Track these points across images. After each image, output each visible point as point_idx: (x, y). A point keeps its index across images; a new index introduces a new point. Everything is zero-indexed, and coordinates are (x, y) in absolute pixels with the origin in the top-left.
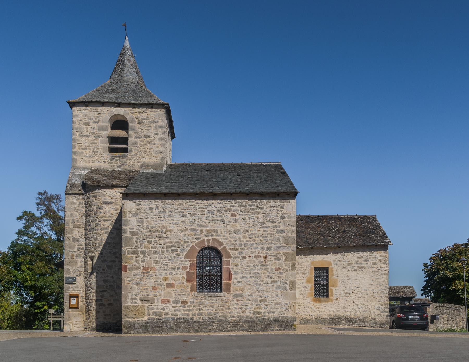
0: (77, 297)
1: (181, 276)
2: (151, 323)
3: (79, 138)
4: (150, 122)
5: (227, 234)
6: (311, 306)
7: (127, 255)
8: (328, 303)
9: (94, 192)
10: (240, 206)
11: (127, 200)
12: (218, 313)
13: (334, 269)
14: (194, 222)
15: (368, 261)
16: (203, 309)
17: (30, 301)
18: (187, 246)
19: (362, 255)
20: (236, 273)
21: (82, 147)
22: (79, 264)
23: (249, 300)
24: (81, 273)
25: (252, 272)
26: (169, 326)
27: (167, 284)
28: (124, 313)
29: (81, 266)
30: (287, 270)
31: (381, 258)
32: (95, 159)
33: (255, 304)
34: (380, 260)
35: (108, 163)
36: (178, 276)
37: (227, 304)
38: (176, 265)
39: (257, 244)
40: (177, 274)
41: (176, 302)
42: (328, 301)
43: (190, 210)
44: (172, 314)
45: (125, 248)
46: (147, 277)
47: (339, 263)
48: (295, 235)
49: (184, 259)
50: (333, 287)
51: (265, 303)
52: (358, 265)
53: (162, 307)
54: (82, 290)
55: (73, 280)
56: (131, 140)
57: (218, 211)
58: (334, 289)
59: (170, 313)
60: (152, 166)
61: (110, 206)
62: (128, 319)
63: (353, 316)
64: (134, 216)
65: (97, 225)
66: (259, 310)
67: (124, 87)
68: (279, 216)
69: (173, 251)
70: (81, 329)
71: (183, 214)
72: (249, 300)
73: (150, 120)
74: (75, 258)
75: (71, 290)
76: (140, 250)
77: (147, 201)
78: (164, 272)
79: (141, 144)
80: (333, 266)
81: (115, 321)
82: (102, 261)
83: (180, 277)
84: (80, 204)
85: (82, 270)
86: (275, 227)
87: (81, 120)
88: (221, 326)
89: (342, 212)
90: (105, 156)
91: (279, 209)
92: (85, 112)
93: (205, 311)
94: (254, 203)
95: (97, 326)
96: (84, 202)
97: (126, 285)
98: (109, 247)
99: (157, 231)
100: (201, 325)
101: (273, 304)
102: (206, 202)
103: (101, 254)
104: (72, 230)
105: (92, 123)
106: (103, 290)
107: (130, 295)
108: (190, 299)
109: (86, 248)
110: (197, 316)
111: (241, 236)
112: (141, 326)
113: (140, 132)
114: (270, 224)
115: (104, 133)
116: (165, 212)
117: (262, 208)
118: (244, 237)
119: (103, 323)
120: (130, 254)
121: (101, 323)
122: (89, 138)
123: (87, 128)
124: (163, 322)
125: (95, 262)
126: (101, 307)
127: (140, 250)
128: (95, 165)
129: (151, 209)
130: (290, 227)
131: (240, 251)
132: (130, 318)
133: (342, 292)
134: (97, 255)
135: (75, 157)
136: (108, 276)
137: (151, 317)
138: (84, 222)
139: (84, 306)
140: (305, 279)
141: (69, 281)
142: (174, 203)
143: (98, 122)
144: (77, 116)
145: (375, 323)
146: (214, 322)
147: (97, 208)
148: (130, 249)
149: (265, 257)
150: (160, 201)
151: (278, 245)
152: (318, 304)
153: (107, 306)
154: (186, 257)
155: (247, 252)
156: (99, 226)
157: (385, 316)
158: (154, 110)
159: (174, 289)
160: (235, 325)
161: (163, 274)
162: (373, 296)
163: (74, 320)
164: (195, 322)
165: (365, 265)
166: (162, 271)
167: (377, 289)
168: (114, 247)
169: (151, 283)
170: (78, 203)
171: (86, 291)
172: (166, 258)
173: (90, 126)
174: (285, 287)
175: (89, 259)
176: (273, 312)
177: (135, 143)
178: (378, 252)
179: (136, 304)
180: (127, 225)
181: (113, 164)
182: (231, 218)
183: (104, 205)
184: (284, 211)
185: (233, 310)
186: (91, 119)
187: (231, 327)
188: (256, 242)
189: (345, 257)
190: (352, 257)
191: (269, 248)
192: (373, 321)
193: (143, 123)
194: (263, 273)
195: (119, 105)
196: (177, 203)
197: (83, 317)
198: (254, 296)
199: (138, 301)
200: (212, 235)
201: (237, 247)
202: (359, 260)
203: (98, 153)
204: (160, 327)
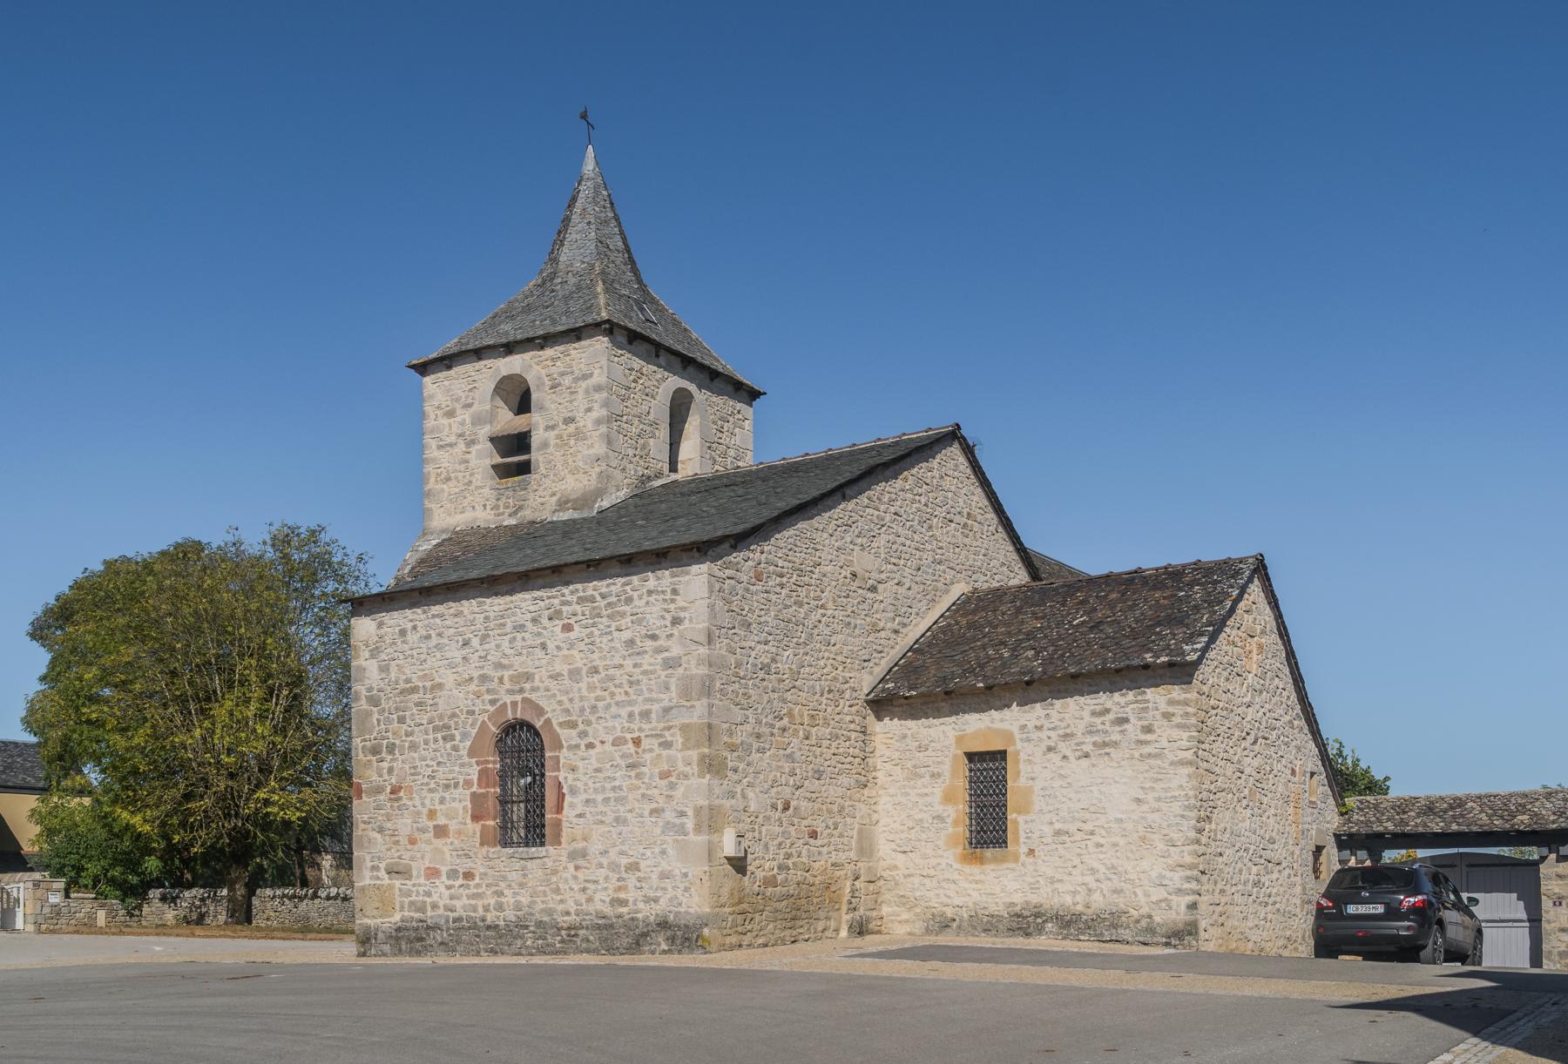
2: (406, 929)
3: (436, 453)
4: (576, 380)
5: (552, 684)
6: (956, 876)
7: (361, 756)
8: (1005, 865)
10: (581, 600)
13: (1023, 756)
15: (1126, 720)
19: (1109, 705)
20: (573, 791)
23: (601, 866)
25: (608, 786)
27: (435, 827)
30: (686, 777)
31: (1171, 709)
34: (1167, 716)
36: (455, 805)
37: (554, 879)
39: (617, 704)
40: (454, 800)
41: (453, 874)
42: (1003, 860)
47: (1035, 735)
50: (1019, 813)
52: (1096, 738)
56: (535, 441)
58: (1021, 819)
59: (441, 904)
60: (575, 501)
63: (1080, 908)
64: (372, 657)
66: (622, 896)
68: (669, 617)
69: (444, 738)
72: (601, 866)
80: (1019, 745)
86: (659, 651)
87: (438, 408)
89: (1151, 560)
90: (486, 491)
91: (668, 596)
93: (509, 899)
94: (613, 588)
99: (414, 690)
100: (499, 936)
101: (654, 876)
105: (460, 405)
107: (368, 858)
108: (479, 869)
110: (495, 913)
111: (583, 685)
114: (649, 643)
117: (629, 600)
118: (591, 688)
124: (428, 927)
131: (581, 727)
133: (1048, 830)
140: (938, 792)
145: (1151, 930)
146: (527, 927)
149: (637, 742)
150: (419, 611)
151: (666, 704)
152: (974, 870)
154: (471, 753)
155: (598, 730)
158: (583, 343)
160: (571, 937)
161: (427, 802)
162: (1143, 839)
164: (489, 928)
165: (1116, 737)
166: (424, 793)
167: (1156, 816)
169: (404, 824)
174: (683, 825)
176: (656, 900)
177: (545, 445)
178: (1159, 689)
184: (680, 602)
185: (567, 895)
186: (457, 400)
187: (562, 941)
188: (618, 698)
189: (1053, 713)
190: (1076, 711)
191: (645, 715)
192: (1144, 923)
194: (632, 788)
195: (509, 348)
198: (613, 853)
199: (382, 873)
200: (521, 691)
202: (1098, 720)
204: (422, 939)
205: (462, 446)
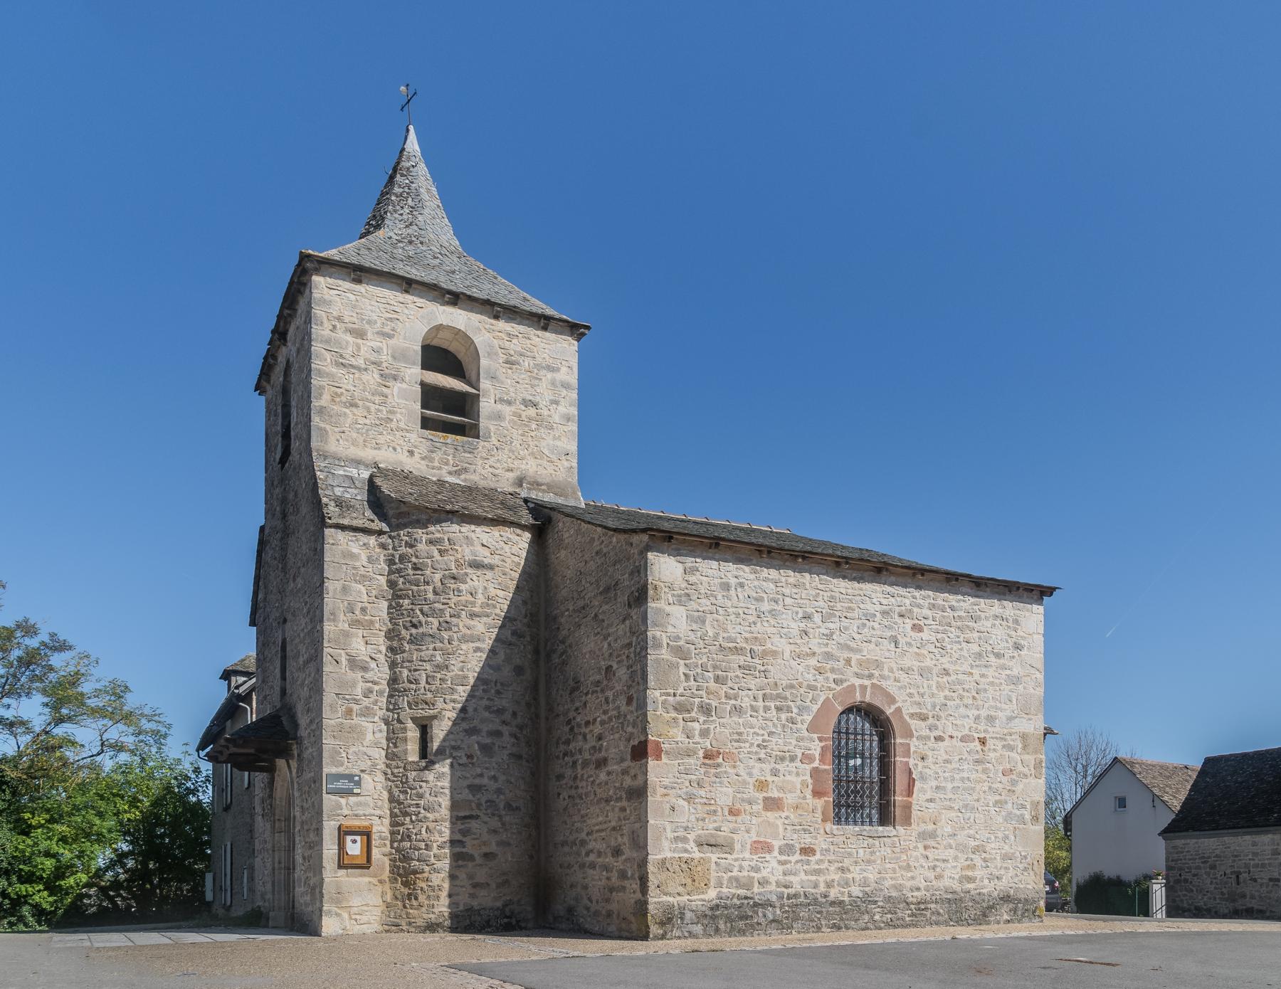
1: (800, 779)
2: (726, 907)
5: (902, 676)
9: (432, 528)
12: (884, 879)
14: (829, 636)
16: (852, 868)
18: (813, 700)
20: (923, 778)
22: (369, 737)
24: (374, 765)
26: (771, 917)
27: (765, 799)
29: (376, 744)
32: (381, 440)
33: (962, 857)
35: (423, 459)
36: (792, 778)
38: (786, 749)
41: (787, 849)
43: (821, 603)
44: (778, 884)
45: (657, 693)
46: (714, 779)
48: (1040, 691)
49: (806, 734)
51: (984, 855)
53: (752, 864)
54: (378, 812)
56: (486, 406)
57: (885, 613)
59: (773, 879)
61: (489, 574)
62: (665, 898)
66: (970, 873)
69: (779, 709)
70: (376, 927)
71: (805, 612)
73: (539, 360)
75: (346, 812)
76: (697, 700)
77: (714, 564)
78: (758, 765)
81: (499, 904)
82: (466, 731)
83: (797, 781)
84: (370, 560)
86: (1004, 667)
88: (890, 912)
90: (413, 437)
92: (352, 297)
93: (855, 873)
94: (962, 604)
95: (453, 916)
97: (658, 798)
99: (738, 651)
100: (845, 912)
102: (856, 584)
103: (463, 710)
104: (346, 635)
106: (467, 814)
108: (821, 843)
112: (701, 917)
116: (759, 600)
118: (939, 687)
119: (467, 910)
121: (461, 908)
122: (366, 377)
124: (756, 905)
126: (460, 863)
127: (697, 700)
129: (726, 587)
130: (1033, 671)
134: (453, 715)
135: (322, 425)
136: (481, 775)
137: (725, 890)
139: (386, 860)
141: (340, 785)
142: (783, 579)
143: (390, 336)
149: (983, 742)
150: (747, 569)
151: (1009, 713)
153: (479, 860)
156: (455, 629)
157: (1033, 883)
158: (547, 334)
159: (784, 815)
160: (920, 912)
161: (756, 772)
163: (356, 902)
164: (833, 903)
168: (498, 692)
171: (393, 815)
172: (763, 729)
175: (410, 725)
179: (686, 855)
180: (662, 625)
181: (436, 464)
182: (913, 634)
183: (469, 571)
191: (990, 719)
195: (455, 299)
196: (791, 580)
198: (961, 837)
199: (692, 846)
200: (870, 676)
201: (924, 711)
203: (394, 425)
204: (747, 917)
205: (372, 378)
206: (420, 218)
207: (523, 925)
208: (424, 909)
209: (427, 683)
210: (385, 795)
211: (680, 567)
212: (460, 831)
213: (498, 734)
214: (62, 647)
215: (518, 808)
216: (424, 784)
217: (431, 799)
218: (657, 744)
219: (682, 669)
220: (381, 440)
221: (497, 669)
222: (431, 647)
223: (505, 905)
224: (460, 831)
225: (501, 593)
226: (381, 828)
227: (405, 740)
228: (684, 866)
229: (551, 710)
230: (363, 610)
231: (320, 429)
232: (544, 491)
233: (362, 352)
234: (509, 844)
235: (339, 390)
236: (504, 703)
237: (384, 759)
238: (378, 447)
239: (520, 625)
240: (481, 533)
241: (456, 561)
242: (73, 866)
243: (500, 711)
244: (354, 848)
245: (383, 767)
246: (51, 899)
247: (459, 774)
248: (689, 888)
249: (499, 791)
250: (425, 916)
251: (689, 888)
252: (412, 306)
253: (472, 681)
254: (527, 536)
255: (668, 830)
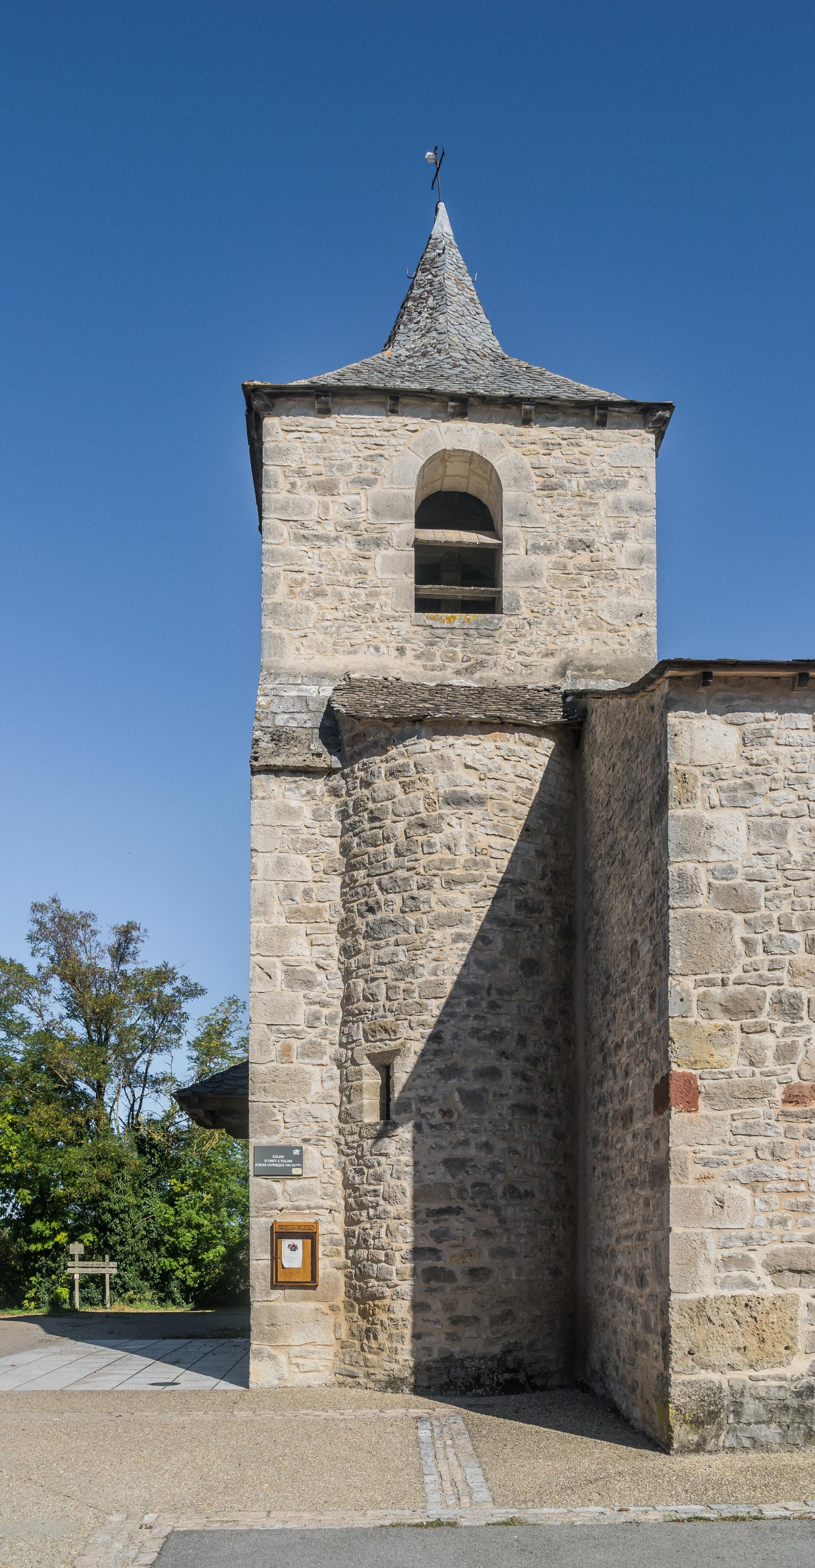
0: (309, 1235)
3: (292, 547)
4: (594, 485)
7: (695, 1016)
9: (393, 752)
11: (697, 710)
17: (15, 1217)
21: (306, 587)
22: (316, 1087)
24: (323, 1130)
28: (679, 1341)
29: (325, 1099)
32: (358, 638)
35: (418, 657)
45: (689, 982)
54: (329, 1203)
55: (287, 1161)
56: (511, 562)
61: (478, 813)
62: (703, 1375)
65: (412, 904)
67: (455, 366)
73: (594, 474)
74: (297, 1063)
75: (282, 1203)
76: (770, 990)
79: (556, 579)
81: (496, 1350)
82: (440, 1072)
84: (317, 816)
85: (327, 1117)
90: (405, 627)
92: (317, 437)
95: (416, 1370)
96: (334, 810)
98: (469, 1004)
103: (435, 1038)
104: (282, 933)
105: (338, 492)
106: (443, 1205)
107: (712, 1239)
109: (347, 1013)
113: (551, 528)
115: (397, 529)
119: (444, 1360)
120: (716, 1011)
121: (435, 1355)
122: (336, 549)
123: (326, 508)
125: (401, 1076)
126: (433, 1284)
127: (770, 990)
128: (364, 664)
132: (713, 1367)
134: (418, 1046)
135: (276, 630)
136: (465, 1143)
138: (338, 900)
141: (274, 1162)
143: (370, 483)
144: (283, 452)
147: (410, 826)
148: (711, 983)
153: (462, 1280)
156: (424, 908)
158: (607, 433)
163: (296, 1338)
168: (493, 1005)
170: (307, 813)
171: (348, 1208)
173: (341, 499)
175: (367, 1066)
179: (747, 1292)
180: (698, 850)
181: (438, 662)
183: (446, 810)
186: (341, 468)
193: (562, 487)
195: (463, 406)
197: (336, 1327)
199: (758, 1273)
203: (375, 614)
205: (347, 547)
206: (442, 319)
207: (539, 1382)
208: (385, 1355)
209: (388, 998)
210: (339, 1176)
211: (734, 734)
212: (433, 1234)
213: (494, 1073)
214: (194, 992)
215: (528, 1194)
216: (383, 1159)
217: (393, 1182)
218: (689, 1080)
219: (740, 932)
220: (358, 638)
221: (491, 966)
222: (392, 940)
223: (507, 1352)
224: (433, 1234)
225: (497, 842)
226: (331, 1227)
227: (360, 1090)
228: (742, 1313)
229: (588, 1029)
230: (307, 893)
231: (274, 637)
232: (599, 677)
233: (332, 514)
234: (512, 1253)
235: (299, 576)
236: (504, 1021)
237: (336, 1122)
238: (353, 649)
239: (531, 892)
240: (463, 748)
241: (427, 797)
242: (214, 1237)
243: (496, 1037)
244: (293, 1257)
245: (335, 1132)
246: (195, 1274)
247: (430, 1142)
248: (752, 1356)
249: (494, 1168)
250: (387, 1366)
251: (752, 1356)
252: (401, 431)
253: (449, 988)
254: (547, 745)
255: (712, 1244)
